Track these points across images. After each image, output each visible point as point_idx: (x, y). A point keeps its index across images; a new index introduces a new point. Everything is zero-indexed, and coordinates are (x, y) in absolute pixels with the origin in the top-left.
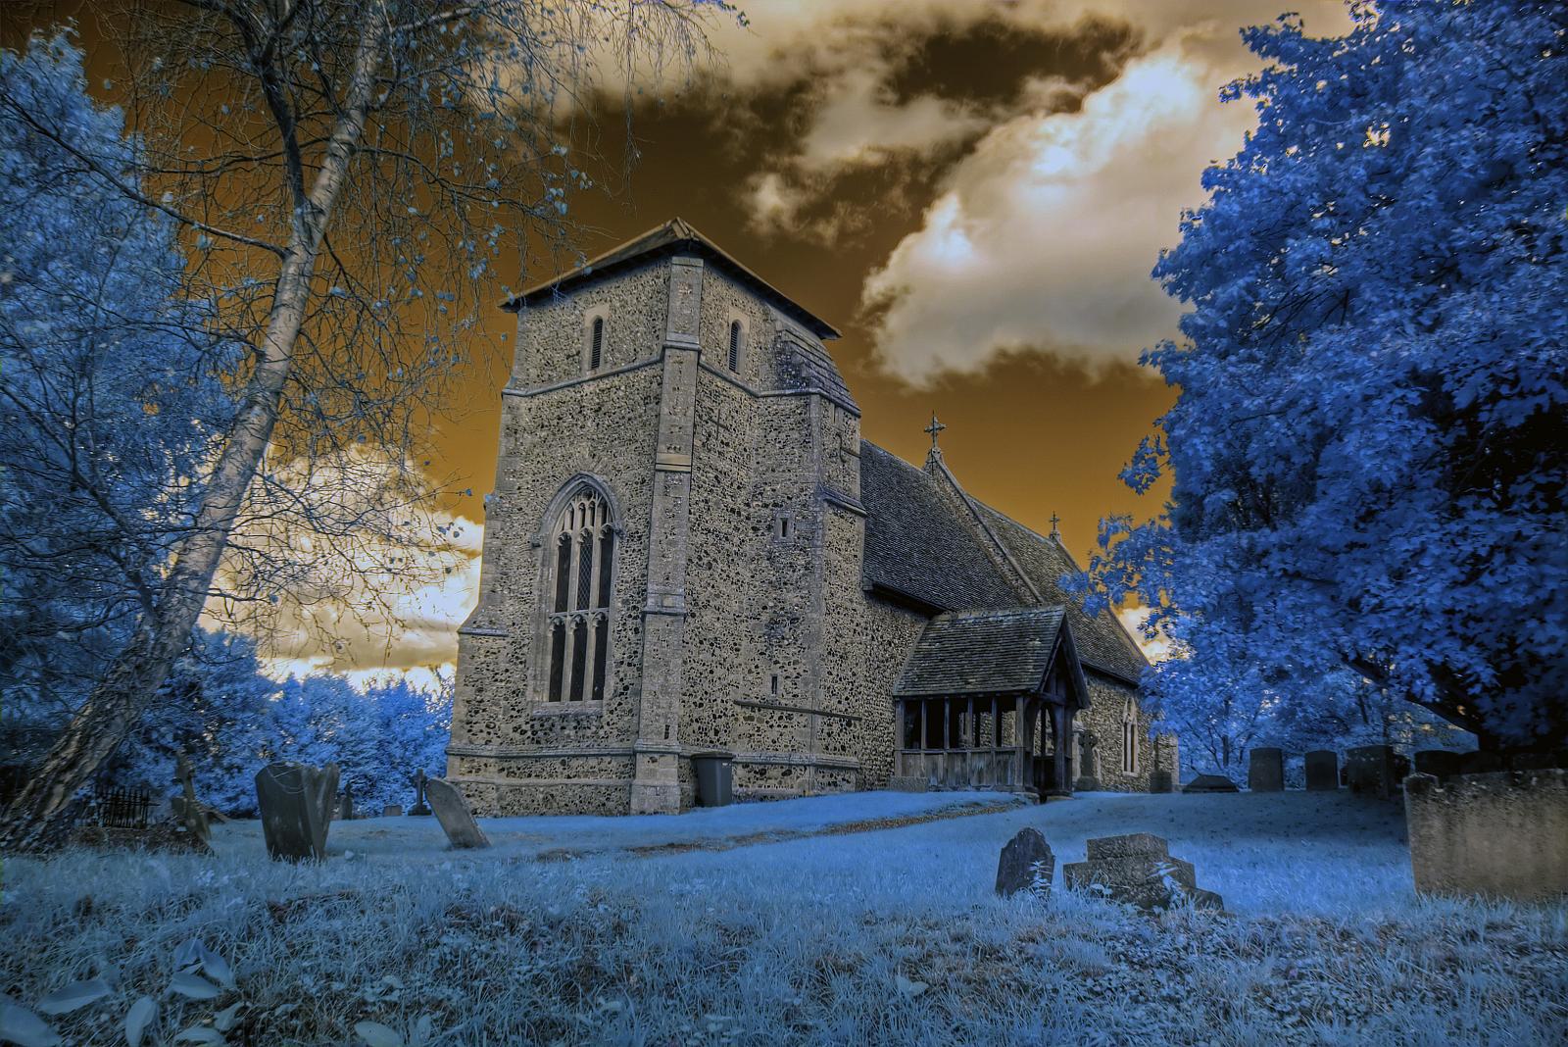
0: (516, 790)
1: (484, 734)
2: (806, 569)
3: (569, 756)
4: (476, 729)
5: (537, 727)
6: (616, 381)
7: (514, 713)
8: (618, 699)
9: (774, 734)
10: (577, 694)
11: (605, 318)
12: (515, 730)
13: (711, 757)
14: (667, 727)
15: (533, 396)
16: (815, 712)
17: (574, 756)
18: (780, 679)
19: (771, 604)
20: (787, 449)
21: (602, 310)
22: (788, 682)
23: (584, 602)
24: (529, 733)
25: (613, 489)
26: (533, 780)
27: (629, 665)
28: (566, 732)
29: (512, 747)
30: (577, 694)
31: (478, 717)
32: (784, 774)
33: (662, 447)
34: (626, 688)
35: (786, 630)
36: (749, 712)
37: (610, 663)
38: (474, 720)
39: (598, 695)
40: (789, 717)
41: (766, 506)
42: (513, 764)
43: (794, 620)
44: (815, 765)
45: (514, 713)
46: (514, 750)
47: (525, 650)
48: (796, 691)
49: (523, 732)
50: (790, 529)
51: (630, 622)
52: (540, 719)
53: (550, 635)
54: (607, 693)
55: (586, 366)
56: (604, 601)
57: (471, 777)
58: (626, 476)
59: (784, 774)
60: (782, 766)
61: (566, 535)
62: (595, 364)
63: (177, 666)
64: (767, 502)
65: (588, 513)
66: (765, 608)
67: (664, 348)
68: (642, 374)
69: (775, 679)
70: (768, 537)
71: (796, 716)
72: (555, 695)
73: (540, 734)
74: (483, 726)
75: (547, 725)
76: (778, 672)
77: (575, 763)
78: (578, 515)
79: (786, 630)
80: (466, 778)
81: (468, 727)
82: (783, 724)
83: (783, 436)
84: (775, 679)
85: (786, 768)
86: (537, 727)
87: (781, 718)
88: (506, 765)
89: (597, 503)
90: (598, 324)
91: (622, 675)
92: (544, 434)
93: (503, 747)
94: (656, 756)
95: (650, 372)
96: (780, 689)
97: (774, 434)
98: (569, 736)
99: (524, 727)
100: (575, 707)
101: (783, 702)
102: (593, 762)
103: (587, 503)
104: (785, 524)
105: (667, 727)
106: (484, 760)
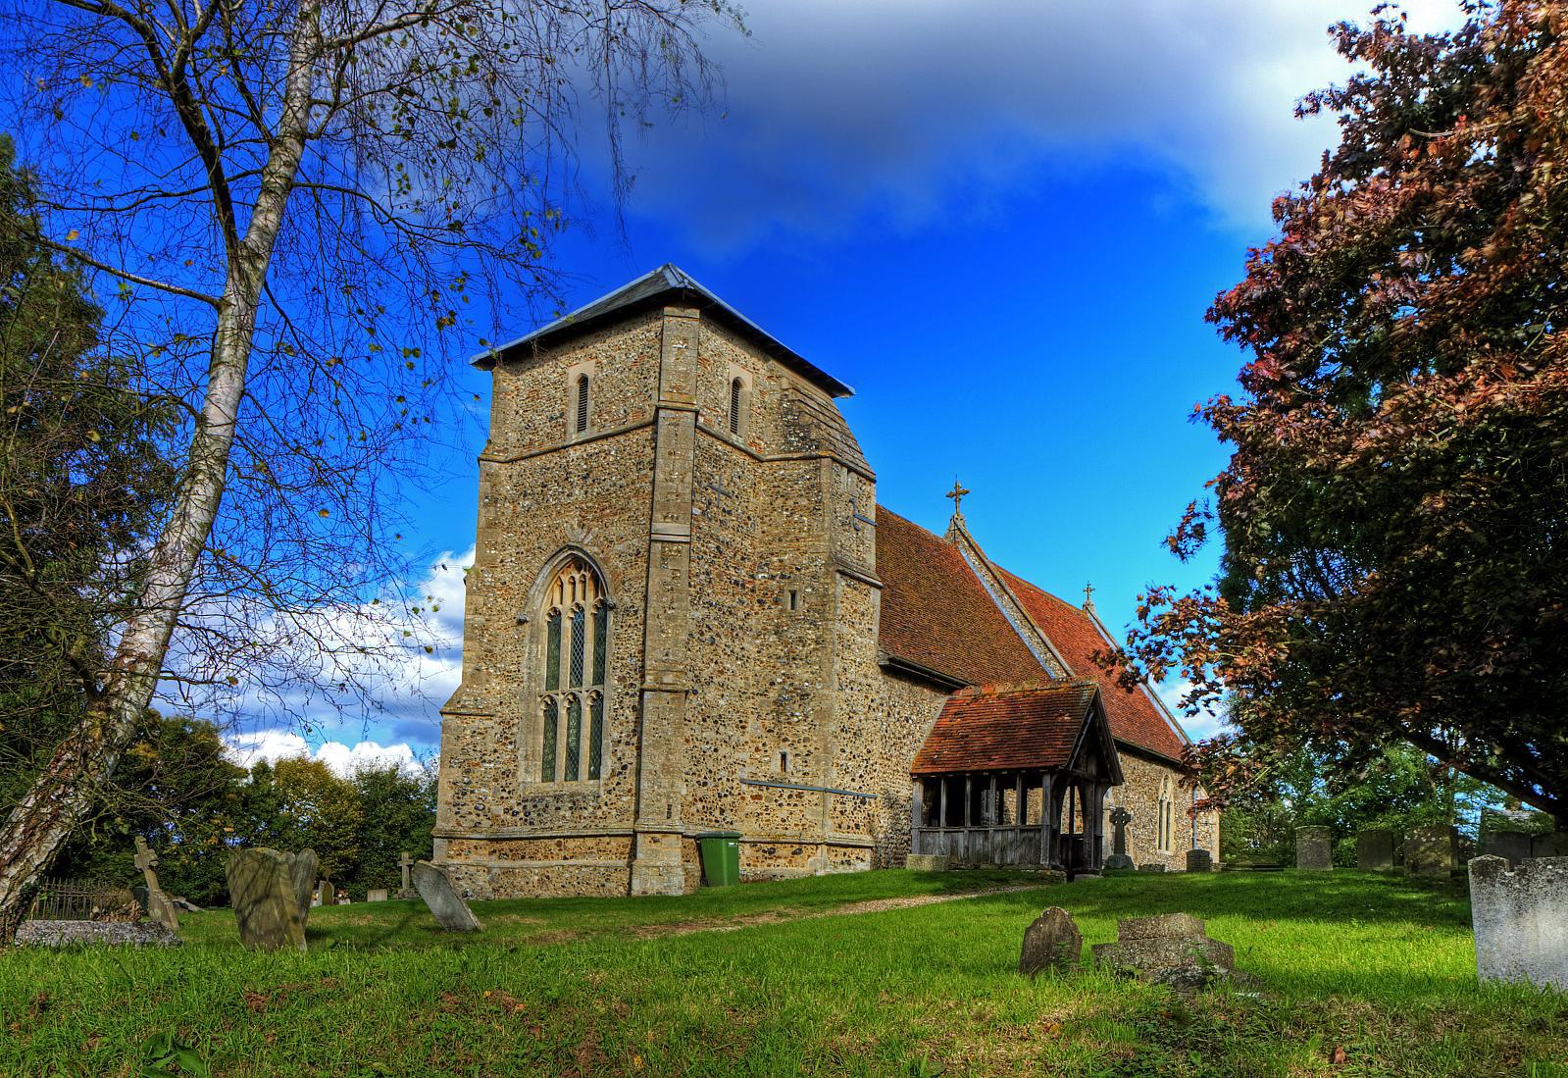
0: (508, 872)
1: (474, 817)
3: (564, 837)
6: (605, 445)
7: (505, 795)
9: (783, 813)
10: (573, 772)
11: (590, 376)
12: (506, 811)
18: (789, 757)
21: (587, 367)
22: (799, 760)
24: (522, 815)
27: (627, 744)
28: (562, 813)
30: (573, 772)
32: (794, 853)
35: (796, 706)
36: (755, 791)
38: (461, 801)
39: (595, 775)
40: (800, 796)
41: (773, 578)
43: (804, 696)
45: (505, 795)
47: (515, 730)
48: (807, 770)
50: (799, 602)
52: (533, 800)
54: (605, 773)
55: (572, 428)
59: (794, 853)
61: (555, 610)
66: (772, 684)
69: (784, 757)
70: (775, 611)
71: (807, 796)
75: (540, 806)
76: (787, 750)
77: (571, 844)
79: (796, 706)
81: (455, 809)
82: (793, 802)
83: (790, 503)
84: (784, 757)
87: (790, 796)
88: (497, 846)
90: (583, 381)
91: (619, 754)
94: (658, 836)
96: (790, 767)
97: (780, 501)
98: (564, 817)
101: (793, 780)
102: (590, 842)
103: (577, 576)
104: (793, 595)
106: (474, 842)
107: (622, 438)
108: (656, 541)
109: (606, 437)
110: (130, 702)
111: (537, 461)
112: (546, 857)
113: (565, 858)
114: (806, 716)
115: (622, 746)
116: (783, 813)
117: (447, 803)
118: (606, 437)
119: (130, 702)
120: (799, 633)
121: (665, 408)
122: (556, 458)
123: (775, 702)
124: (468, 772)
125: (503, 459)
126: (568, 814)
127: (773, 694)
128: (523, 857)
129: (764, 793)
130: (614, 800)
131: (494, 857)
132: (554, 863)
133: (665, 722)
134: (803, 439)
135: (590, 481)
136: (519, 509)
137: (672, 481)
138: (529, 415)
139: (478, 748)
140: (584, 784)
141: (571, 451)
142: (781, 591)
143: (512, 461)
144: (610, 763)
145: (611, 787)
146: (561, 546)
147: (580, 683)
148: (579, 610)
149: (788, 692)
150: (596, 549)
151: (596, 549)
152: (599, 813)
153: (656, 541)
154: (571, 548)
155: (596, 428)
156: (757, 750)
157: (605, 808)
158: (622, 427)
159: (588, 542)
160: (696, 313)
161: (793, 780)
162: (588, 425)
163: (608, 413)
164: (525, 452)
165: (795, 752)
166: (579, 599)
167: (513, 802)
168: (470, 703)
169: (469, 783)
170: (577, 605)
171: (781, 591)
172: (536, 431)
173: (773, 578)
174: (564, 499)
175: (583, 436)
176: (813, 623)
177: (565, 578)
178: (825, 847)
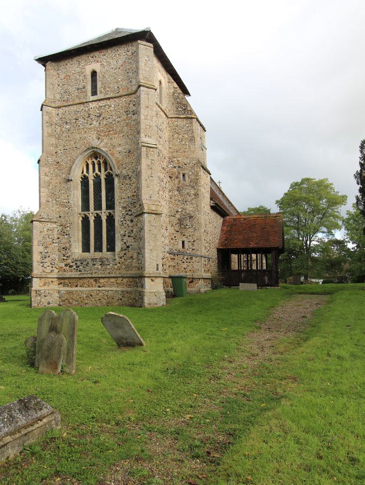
0: (69, 293)
1: (50, 268)
2: (195, 195)
3: (98, 278)
4: (46, 265)
5: (79, 263)
6: (108, 102)
7: (65, 258)
8: (124, 252)
9: (185, 265)
10: (99, 248)
11: (98, 71)
12: (66, 265)
13: (182, 277)
14: (157, 265)
15: (59, 107)
16: (202, 257)
17: (101, 277)
18: (186, 243)
19: (180, 210)
20: (183, 142)
21: (97, 67)
22: (190, 244)
23: (98, 206)
24: (75, 267)
25: (113, 154)
26: (78, 288)
27: (129, 236)
28: (96, 266)
29: (65, 273)
30: (99, 248)
31: (47, 260)
32: (190, 282)
33: (142, 135)
34: (128, 247)
35: (188, 221)
36: (172, 256)
37: (118, 236)
38: (44, 261)
39: (111, 248)
40: (191, 258)
41: (175, 167)
42: (66, 281)
43: (191, 217)
44: (204, 279)
45: (65, 258)
46: (68, 275)
47: (68, 229)
48: (194, 248)
49: (71, 266)
50: (187, 178)
51: (127, 217)
52: (80, 260)
53: (80, 222)
54: (118, 248)
55: (89, 94)
56: (111, 206)
57: (46, 287)
58: (120, 149)
59: (190, 282)
60: (189, 279)
61: (85, 176)
62: (94, 93)
63: (311, 265)
64: (176, 165)
65: (91, 167)
66: (177, 212)
67: (140, 86)
68: (123, 99)
69: (183, 242)
70: (177, 181)
71: (194, 258)
72: (86, 248)
73: (81, 267)
74: (49, 264)
75: (84, 263)
76: (185, 239)
77: (102, 281)
78: (91, 167)
79: (188, 221)
80: (43, 288)
81: (42, 264)
82: (188, 261)
83: (181, 136)
84: (183, 242)
85: (191, 280)
86: (79, 263)
87: (187, 259)
88: (62, 281)
89: (102, 161)
90: (94, 74)
91: (125, 241)
92: (67, 127)
93: (61, 273)
94: (154, 278)
95: (128, 99)
96: (186, 246)
97: (176, 136)
98: (98, 268)
99: (71, 264)
100: (98, 255)
101: (188, 252)
102: (113, 280)
103: (96, 162)
104: (184, 175)
105: (157, 265)
106: (51, 280)
107: (117, 100)
108: (144, 146)
109: (109, 99)
110: (247, 259)
111: (72, 108)
112: (89, 286)
113: (99, 287)
114: (192, 226)
115: (126, 238)
116: (185, 265)
117: (38, 262)
118: (109, 99)
119: (247, 259)
120: (187, 191)
121: (143, 86)
122: (82, 107)
123: (179, 219)
124: (46, 247)
125: (54, 106)
126: (100, 267)
127: (178, 216)
128: (77, 286)
129: (176, 257)
130: (123, 261)
131: (61, 286)
132: (95, 289)
133: (154, 227)
134: (185, 109)
135: (101, 118)
136: (64, 129)
137: (148, 119)
138: (66, 86)
139: (50, 237)
140: (105, 253)
141: (90, 104)
142: (179, 173)
143: (59, 107)
144: (120, 245)
145: (121, 255)
146: (88, 146)
147: (88, 210)
148: (97, 177)
149: (184, 215)
150: (107, 149)
151: (107, 149)
152: (116, 267)
153: (144, 146)
154: (93, 148)
155: (103, 94)
156: (172, 239)
157: (119, 265)
158: (117, 95)
159: (103, 146)
160: (151, 45)
161: (188, 252)
162: (98, 92)
163: (109, 88)
164: (65, 104)
165: (188, 240)
166: (97, 171)
167: (69, 261)
168: (45, 216)
169: (47, 252)
170: (96, 174)
171: (179, 173)
172: (70, 94)
173: (175, 167)
174: (88, 126)
175: (95, 98)
176: (193, 187)
177: (90, 162)
178: (202, 280)
